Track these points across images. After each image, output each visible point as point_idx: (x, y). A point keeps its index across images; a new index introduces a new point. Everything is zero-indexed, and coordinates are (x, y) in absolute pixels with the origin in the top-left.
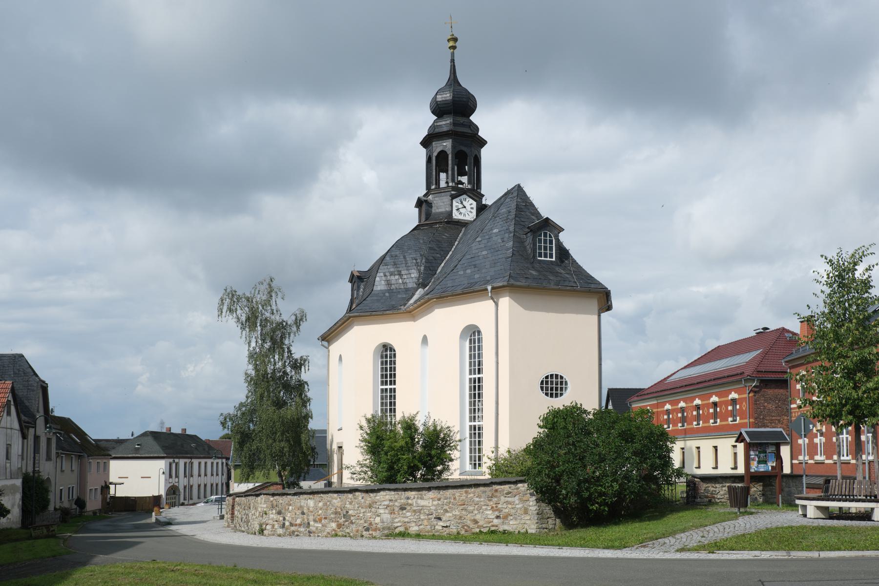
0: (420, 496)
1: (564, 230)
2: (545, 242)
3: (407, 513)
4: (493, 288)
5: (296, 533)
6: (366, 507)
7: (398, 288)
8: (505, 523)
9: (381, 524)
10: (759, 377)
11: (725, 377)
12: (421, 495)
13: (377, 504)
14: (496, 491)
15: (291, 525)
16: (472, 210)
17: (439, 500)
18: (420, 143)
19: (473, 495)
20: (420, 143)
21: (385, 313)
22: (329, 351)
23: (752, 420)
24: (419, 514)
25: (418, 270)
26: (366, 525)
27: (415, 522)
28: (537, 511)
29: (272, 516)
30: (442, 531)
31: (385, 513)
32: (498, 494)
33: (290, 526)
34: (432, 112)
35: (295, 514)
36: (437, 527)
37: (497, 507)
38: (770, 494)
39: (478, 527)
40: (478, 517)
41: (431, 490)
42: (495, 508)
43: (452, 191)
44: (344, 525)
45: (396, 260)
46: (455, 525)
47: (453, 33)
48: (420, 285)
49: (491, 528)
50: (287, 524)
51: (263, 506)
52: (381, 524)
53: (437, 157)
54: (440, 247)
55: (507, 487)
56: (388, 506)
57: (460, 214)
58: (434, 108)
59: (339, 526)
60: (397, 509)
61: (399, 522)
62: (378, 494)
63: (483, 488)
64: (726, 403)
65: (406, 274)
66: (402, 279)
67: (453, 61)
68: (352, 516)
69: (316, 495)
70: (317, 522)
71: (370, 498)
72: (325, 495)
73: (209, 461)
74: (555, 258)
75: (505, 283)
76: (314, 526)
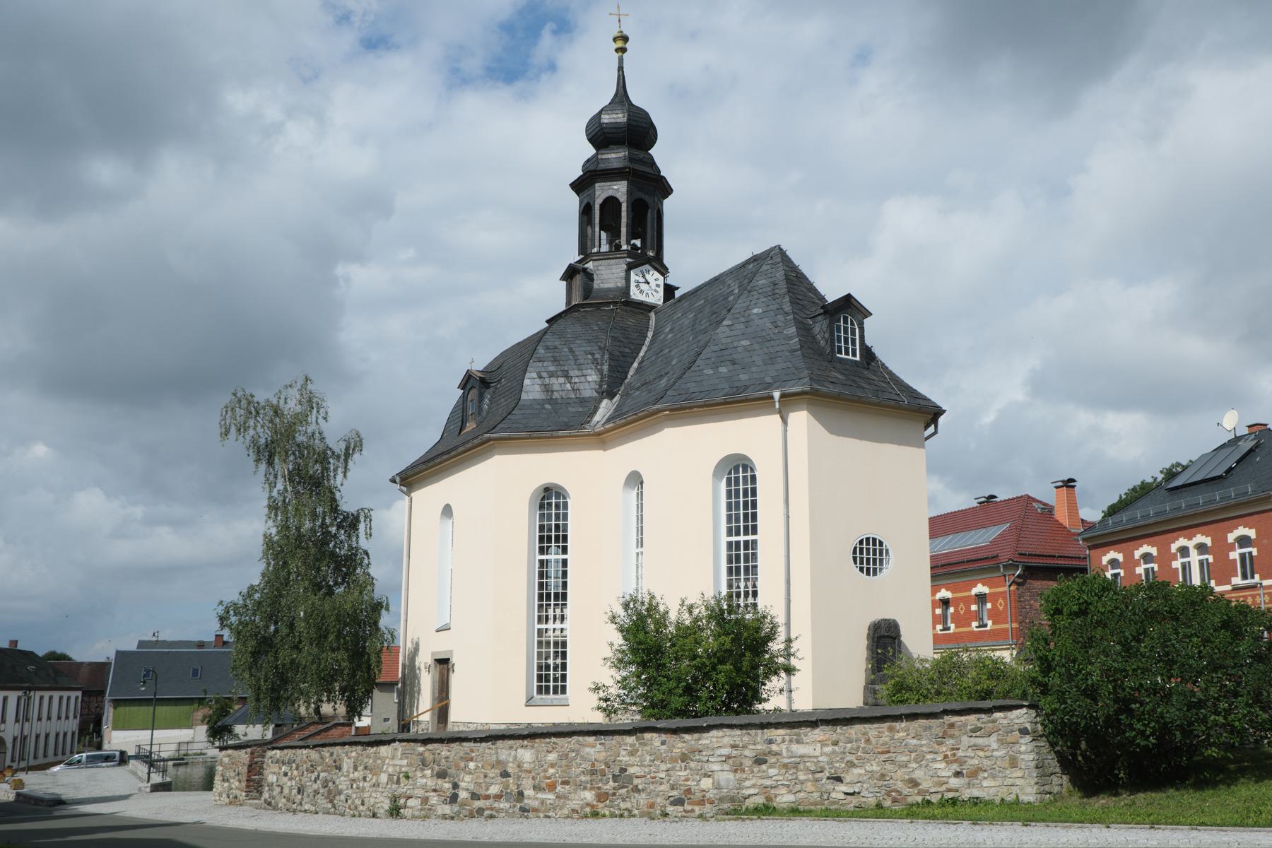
0: (795, 737)
2: (846, 332)
3: (770, 771)
4: (782, 396)
5: (487, 813)
6: (673, 760)
7: (564, 397)
8: (974, 785)
9: (715, 792)
10: (1024, 562)
12: (799, 735)
13: (704, 753)
14: (952, 726)
15: (475, 796)
16: (657, 288)
17: (835, 743)
18: (570, 185)
19: (905, 734)
20: (570, 185)
22: (411, 499)
23: (1015, 625)
25: (599, 370)
27: (788, 786)
28: (1035, 762)
29: (421, 781)
30: (845, 802)
32: (955, 732)
34: (590, 140)
35: (485, 776)
37: (954, 755)
39: (919, 794)
40: (918, 774)
42: (951, 758)
43: (628, 257)
45: (555, 354)
46: (871, 790)
47: (622, 29)
48: (605, 394)
49: (946, 794)
50: (463, 795)
51: (398, 762)
52: (715, 792)
53: (602, 206)
54: (628, 338)
55: (972, 718)
58: (593, 134)
59: (602, 797)
60: (748, 763)
61: (754, 786)
62: (706, 735)
64: (968, 601)
65: (578, 376)
66: (570, 383)
67: (621, 68)
68: (637, 777)
69: (537, 740)
70: (544, 789)
73: (56, 695)
75: (807, 388)
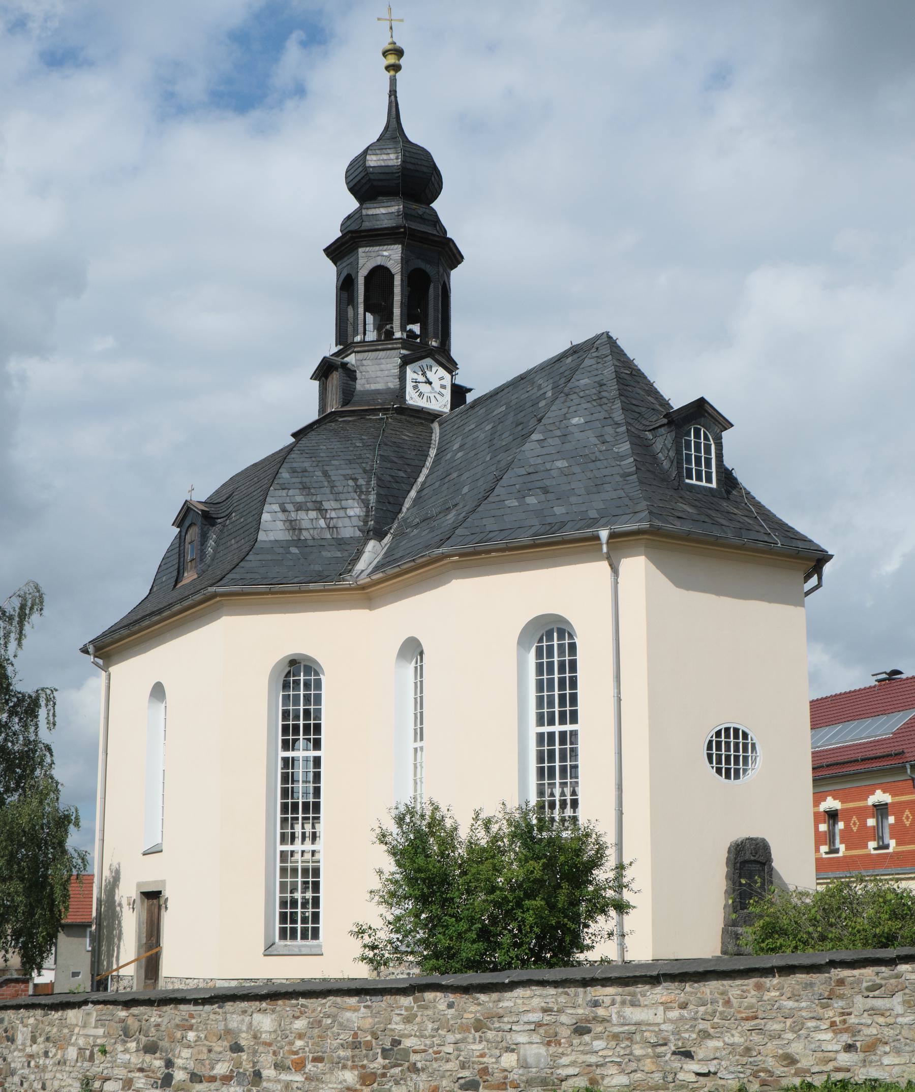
0: (629, 998)
1: (732, 426)
2: (698, 449)
3: (595, 1043)
4: (612, 536)
6: (464, 1029)
7: (316, 537)
9: (521, 1072)
11: (823, 767)
12: (633, 995)
13: (506, 1020)
14: (841, 982)
16: (443, 391)
17: (684, 1006)
18: (325, 250)
19: (777, 994)
20: (325, 250)
21: (304, 587)
24: (628, 1043)
25: (363, 500)
26: (466, 1073)
27: (619, 1064)
30: (696, 1085)
31: (531, 1043)
32: (846, 990)
33: (191, 1081)
35: (210, 1051)
36: (681, 1076)
37: (845, 1021)
39: (796, 1074)
40: (796, 1048)
41: (659, 983)
42: (841, 1026)
43: (403, 348)
44: (384, 1075)
45: (304, 480)
46: (732, 1069)
47: (395, 40)
48: (371, 533)
52: (521, 1072)
53: (367, 279)
55: (868, 972)
56: (541, 1026)
57: (419, 396)
60: (565, 1032)
61: (573, 1064)
63: (804, 976)
66: (325, 518)
67: (393, 93)
68: (415, 1052)
69: (280, 1002)
70: (289, 1068)
71: (479, 1004)
72: (312, 1001)
74: (718, 483)
75: (645, 525)
76: (279, 1081)
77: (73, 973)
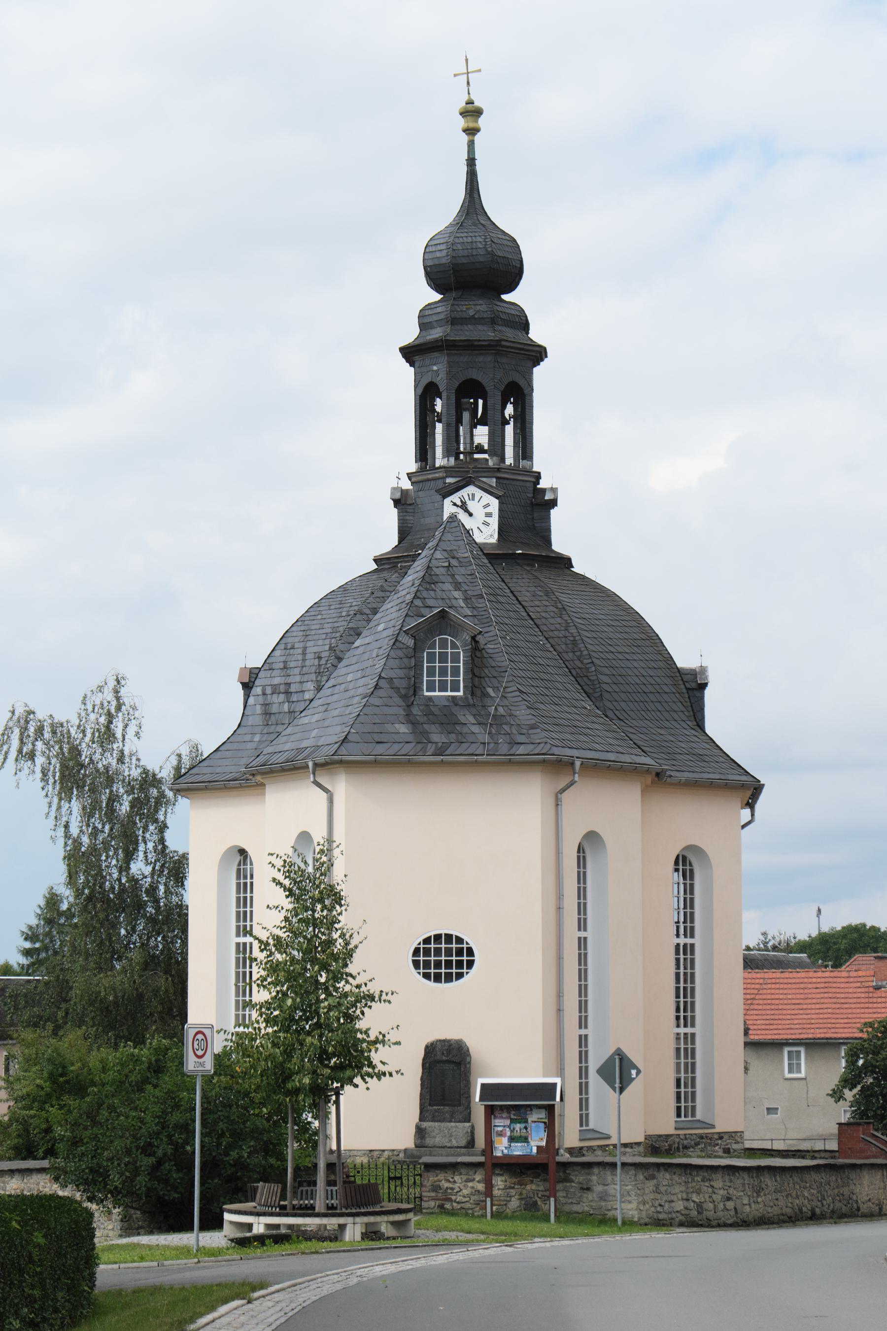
16: (488, 520)
38: (564, 1197)
67: (471, 162)
74: (464, 692)
77: (768, 1109)
